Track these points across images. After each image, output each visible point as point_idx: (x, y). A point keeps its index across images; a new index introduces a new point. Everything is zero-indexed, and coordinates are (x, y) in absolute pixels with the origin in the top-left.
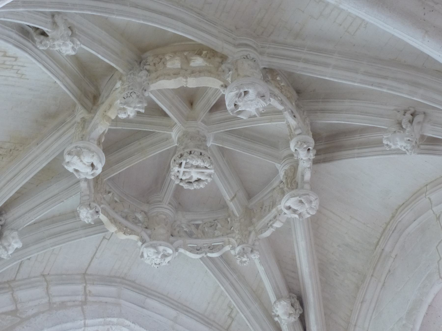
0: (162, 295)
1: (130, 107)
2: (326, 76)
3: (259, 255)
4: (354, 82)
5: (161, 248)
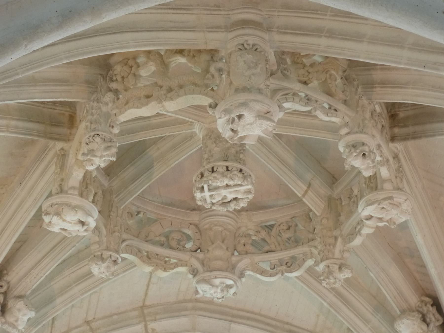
0: (252, 313)
1: (96, 156)
2: (359, 57)
3: (350, 273)
4: (399, 63)
5: (217, 281)
